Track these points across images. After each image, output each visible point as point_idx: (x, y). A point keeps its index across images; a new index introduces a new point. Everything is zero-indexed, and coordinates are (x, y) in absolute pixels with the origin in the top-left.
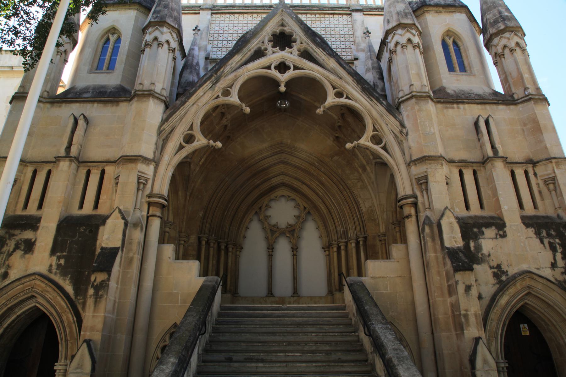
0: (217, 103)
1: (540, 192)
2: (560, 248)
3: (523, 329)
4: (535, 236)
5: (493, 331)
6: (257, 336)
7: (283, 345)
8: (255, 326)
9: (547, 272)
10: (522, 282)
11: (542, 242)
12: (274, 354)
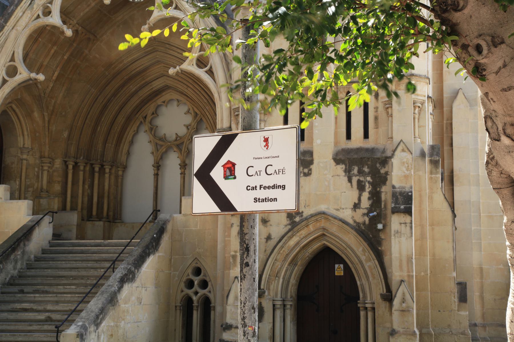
0: (37, 25)
1: (376, 118)
2: (369, 187)
3: (338, 269)
4: (344, 174)
5: (276, 271)
6: (57, 271)
7: (70, 279)
8: (61, 262)
9: (347, 214)
10: (317, 223)
11: (350, 180)
12: (56, 287)
